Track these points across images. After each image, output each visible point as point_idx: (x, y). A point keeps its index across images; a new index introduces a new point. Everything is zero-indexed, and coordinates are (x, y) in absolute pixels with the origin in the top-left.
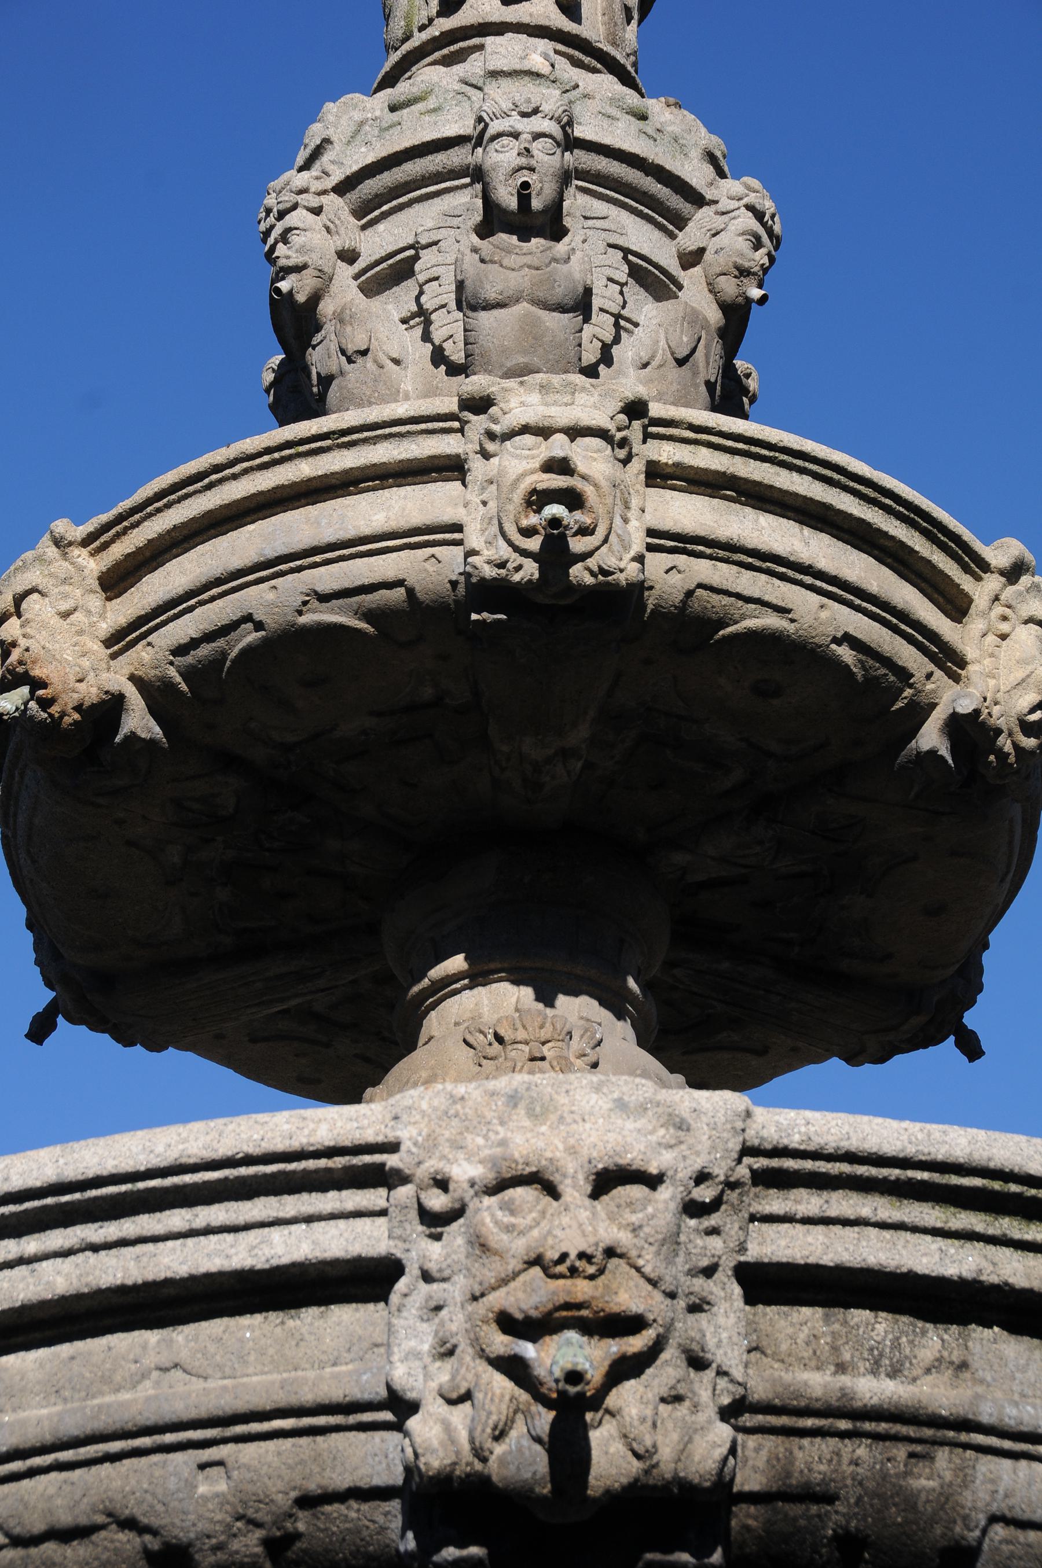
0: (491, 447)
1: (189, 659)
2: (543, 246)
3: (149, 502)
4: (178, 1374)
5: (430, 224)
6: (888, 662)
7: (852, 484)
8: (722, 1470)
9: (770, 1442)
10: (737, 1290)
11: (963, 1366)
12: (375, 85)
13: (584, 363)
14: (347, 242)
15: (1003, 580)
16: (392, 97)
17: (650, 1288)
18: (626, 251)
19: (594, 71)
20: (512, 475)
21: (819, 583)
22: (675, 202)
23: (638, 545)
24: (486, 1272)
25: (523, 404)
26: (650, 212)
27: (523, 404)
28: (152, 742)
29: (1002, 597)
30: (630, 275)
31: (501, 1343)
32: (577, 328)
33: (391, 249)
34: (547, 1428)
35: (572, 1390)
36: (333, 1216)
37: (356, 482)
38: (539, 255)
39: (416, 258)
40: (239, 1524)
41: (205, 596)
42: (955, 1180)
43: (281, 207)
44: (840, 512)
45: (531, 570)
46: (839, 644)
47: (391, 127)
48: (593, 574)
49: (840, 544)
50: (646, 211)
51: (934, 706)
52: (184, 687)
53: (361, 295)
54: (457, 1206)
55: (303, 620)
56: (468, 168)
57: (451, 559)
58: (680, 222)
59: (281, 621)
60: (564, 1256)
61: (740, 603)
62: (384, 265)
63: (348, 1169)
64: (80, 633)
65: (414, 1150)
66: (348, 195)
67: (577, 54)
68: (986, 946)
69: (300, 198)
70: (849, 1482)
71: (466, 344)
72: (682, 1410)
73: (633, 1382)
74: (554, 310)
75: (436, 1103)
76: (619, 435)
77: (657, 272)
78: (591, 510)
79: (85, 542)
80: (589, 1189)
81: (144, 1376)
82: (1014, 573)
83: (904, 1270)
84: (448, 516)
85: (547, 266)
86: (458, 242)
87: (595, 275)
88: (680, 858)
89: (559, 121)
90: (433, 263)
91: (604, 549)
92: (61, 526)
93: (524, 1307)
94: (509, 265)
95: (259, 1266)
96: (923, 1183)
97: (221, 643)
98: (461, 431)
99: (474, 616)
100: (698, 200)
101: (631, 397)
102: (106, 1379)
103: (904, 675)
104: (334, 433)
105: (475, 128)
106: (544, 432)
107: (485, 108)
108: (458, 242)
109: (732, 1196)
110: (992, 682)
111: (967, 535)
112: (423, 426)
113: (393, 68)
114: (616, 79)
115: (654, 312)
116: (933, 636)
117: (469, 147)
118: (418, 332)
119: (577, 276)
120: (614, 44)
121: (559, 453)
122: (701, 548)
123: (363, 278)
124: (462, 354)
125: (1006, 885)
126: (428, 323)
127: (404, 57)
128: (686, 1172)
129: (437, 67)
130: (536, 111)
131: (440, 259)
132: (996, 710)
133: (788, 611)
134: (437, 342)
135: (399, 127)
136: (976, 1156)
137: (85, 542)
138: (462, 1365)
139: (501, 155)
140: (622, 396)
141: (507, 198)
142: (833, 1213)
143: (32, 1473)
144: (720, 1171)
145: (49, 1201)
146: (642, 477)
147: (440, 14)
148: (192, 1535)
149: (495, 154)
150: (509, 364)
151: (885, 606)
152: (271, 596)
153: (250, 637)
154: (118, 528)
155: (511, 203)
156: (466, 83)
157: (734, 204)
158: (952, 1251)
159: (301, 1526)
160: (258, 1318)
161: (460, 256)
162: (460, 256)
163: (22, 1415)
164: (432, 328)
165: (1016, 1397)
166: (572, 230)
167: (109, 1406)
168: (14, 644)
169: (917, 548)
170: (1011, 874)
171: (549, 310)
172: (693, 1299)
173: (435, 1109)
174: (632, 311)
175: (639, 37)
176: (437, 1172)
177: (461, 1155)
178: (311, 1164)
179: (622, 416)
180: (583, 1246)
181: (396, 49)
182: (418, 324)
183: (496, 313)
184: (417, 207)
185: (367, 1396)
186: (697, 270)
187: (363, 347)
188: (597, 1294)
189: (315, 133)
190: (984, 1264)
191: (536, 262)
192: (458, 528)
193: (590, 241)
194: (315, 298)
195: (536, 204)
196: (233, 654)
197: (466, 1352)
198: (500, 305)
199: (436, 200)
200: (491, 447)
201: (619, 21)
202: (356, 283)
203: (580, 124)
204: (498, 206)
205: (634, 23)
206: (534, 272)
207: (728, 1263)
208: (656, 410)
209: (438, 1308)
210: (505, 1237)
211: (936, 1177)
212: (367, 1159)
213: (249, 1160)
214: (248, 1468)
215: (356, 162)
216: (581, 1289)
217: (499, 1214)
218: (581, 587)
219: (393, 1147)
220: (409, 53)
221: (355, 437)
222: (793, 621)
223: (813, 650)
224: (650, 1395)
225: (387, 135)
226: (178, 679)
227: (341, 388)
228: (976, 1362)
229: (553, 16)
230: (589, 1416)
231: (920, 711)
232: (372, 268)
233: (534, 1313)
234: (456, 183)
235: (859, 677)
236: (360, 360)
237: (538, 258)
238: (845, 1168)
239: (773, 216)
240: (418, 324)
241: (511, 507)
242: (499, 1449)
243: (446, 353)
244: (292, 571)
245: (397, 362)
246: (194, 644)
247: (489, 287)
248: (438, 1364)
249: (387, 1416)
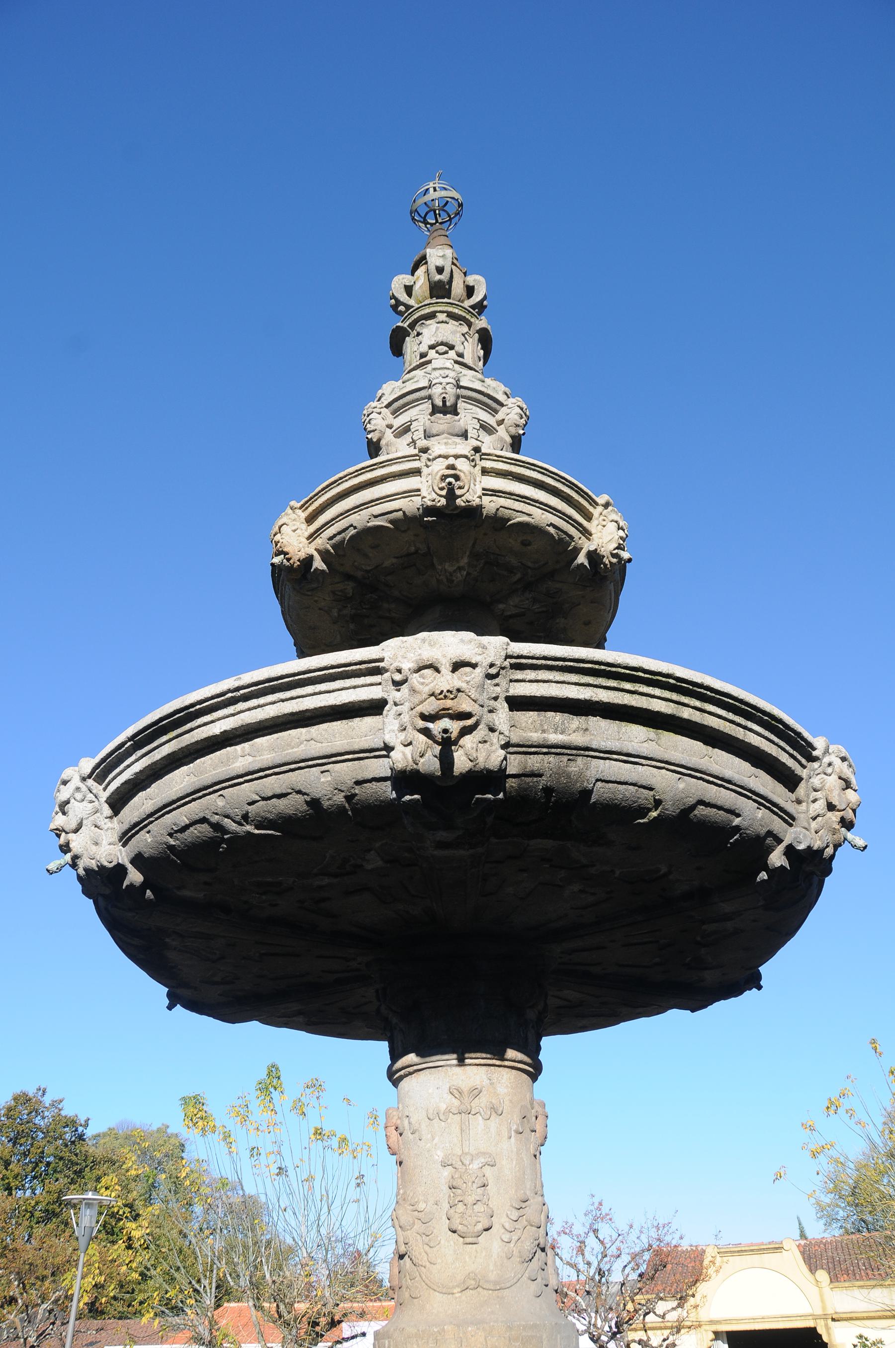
0: (429, 463)
1: (333, 541)
3: (320, 492)
4: (312, 742)
6: (566, 533)
7: (551, 475)
8: (501, 765)
9: (519, 757)
10: (506, 705)
11: (586, 730)
15: (603, 508)
17: (474, 703)
18: (479, 420)
20: (436, 471)
21: (541, 506)
22: (494, 405)
23: (480, 492)
24: (415, 699)
25: (439, 449)
27: (439, 449)
28: (323, 571)
29: (603, 514)
30: (480, 427)
31: (421, 724)
34: (438, 752)
35: (445, 736)
36: (363, 686)
37: (385, 479)
39: (411, 424)
40: (336, 791)
41: (338, 520)
42: (582, 665)
43: (368, 413)
44: (547, 484)
45: (443, 501)
46: (549, 526)
48: (464, 502)
49: (548, 494)
51: (582, 548)
52: (332, 551)
54: (405, 678)
55: (369, 525)
57: (417, 502)
58: (496, 412)
59: (362, 525)
60: (442, 692)
61: (515, 512)
62: (401, 428)
63: (367, 669)
64: (299, 536)
65: (389, 660)
68: (605, 640)
69: (374, 410)
70: (547, 769)
72: (487, 745)
73: (469, 736)
75: (396, 644)
76: (471, 458)
78: (463, 481)
79: (300, 508)
80: (451, 669)
81: (301, 743)
82: (606, 505)
83: (565, 697)
84: (415, 487)
88: (501, 606)
89: (455, 379)
91: (468, 493)
92: (293, 503)
93: (429, 710)
95: (338, 704)
96: (571, 666)
97: (343, 535)
98: (419, 460)
99: (425, 519)
100: (502, 405)
101: (475, 446)
102: (289, 745)
103: (571, 537)
106: (446, 457)
109: (502, 672)
110: (601, 540)
111: (590, 493)
112: (407, 459)
116: (580, 525)
119: (462, 425)
121: (451, 463)
122: (501, 494)
125: (610, 615)
126: (415, 444)
128: (486, 663)
130: (447, 376)
132: (602, 549)
133: (531, 515)
136: (589, 656)
137: (300, 508)
138: (408, 733)
141: (439, 403)
142: (539, 678)
143: (266, 776)
144: (498, 663)
145: (267, 685)
146: (480, 471)
148: (320, 795)
151: (564, 514)
152: (358, 517)
153: (352, 532)
154: (311, 502)
155: (441, 404)
157: (513, 405)
158: (582, 690)
159: (357, 791)
160: (339, 722)
163: (262, 757)
165: (605, 739)
167: (290, 753)
168: (278, 542)
169: (574, 496)
170: (612, 610)
172: (490, 708)
173: (396, 646)
176: (397, 667)
177: (405, 660)
178: (354, 667)
179: (472, 451)
180: (448, 688)
184: (411, 410)
185: (376, 746)
186: (502, 426)
188: (454, 705)
189: (380, 392)
190: (593, 694)
192: (419, 490)
194: (379, 440)
195: (448, 404)
196: (347, 539)
197: (410, 729)
198: (437, 435)
200: (429, 463)
207: (502, 696)
208: (484, 450)
209: (400, 715)
210: (421, 687)
211: (576, 664)
212: (374, 665)
213: (333, 667)
214: (337, 772)
216: (448, 703)
217: (419, 679)
218: (460, 507)
219: (381, 660)
221: (385, 464)
222: (533, 518)
223: (540, 528)
224: (475, 740)
226: (330, 548)
228: (591, 729)
230: (453, 748)
231: (577, 551)
233: (432, 713)
235: (557, 538)
238: (543, 662)
239: (526, 409)
241: (435, 481)
242: (422, 760)
244: (365, 508)
246: (335, 536)
248: (401, 733)
249: (384, 753)
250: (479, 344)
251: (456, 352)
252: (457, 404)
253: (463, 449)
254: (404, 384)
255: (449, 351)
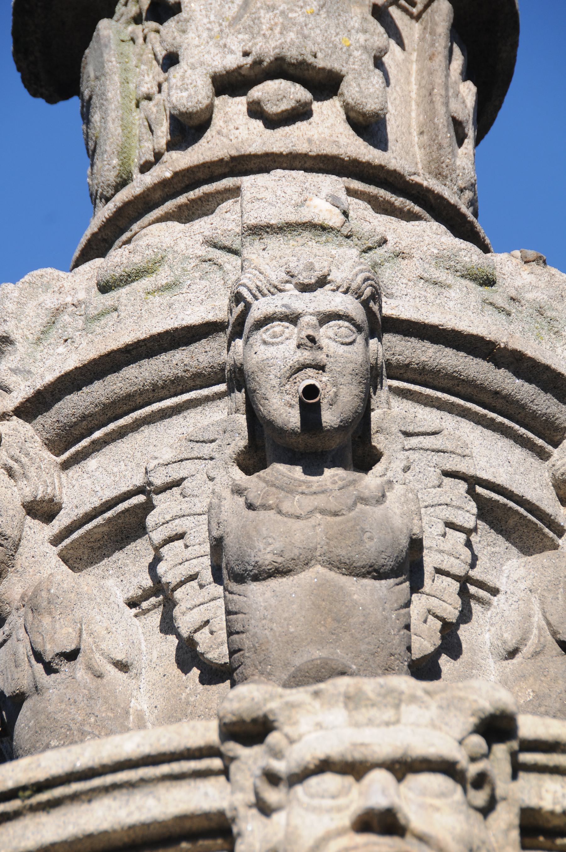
2: (342, 479)
5: (168, 455)
12: (77, 253)
13: (416, 654)
14: (41, 489)
16: (102, 272)
19: (410, 217)
25: (319, 726)
26: (506, 421)
27: (319, 726)
30: (481, 516)
32: (402, 601)
33: (108, 494)
38: (337, 493)
39: (148, 507)
47: (102, 314)
50: (500, 419)
53: (65, 567)
56: (223, 370)
62: (99, 520)
66: (40, 419)
67: (382, 193)
71: (230, 634)
74: (364, 576)
76: (473, 770)
77: (522, 510)
85: (350, 509)
86: (212, 479)
87: (426, 519)
90: (174, 512)
94: (291, 511)
98: (225, 772)
104: (24, 788)
105: (231, 311)
107: (245, 281)
108: (212, 479)
112: (165, 769)
113: (103, 227)
114: (443, 227)
115: (522, 572)
117: (223, 338)
118: (155, 618)
119: (398, 522)
120: (439, 175)
123: (67, 541)
124: (225, 650)
127: (120, 211)
129: (170, 223)
130: (322, 282)
131: (184, 506)
134: (185, 632)
135: (115, 314)
139: (272, 349)
140: (475, 706)
146: (515, 834)
147: (171, 146)
149: (263, 347)
150: (298, 661)
156: (215, 246)
161: (215, 501)
162: (215, 501)
164: (177, 612)
166: (386, 453)
171: (357, 575)
174: (486, 571)
175: (477, 161)
181: (108, 200)
182: (155, 607)
183: (274, 583)
184: (146, 431)
187: (69, 648)
191: (333, 505)
193: (415, 468)
199: (177, 420)
201: (445, 142)
202: (56, 550)
203: (390, 296)
204: (270, 423)
205: (469, 143)
206: (330, 519)
215: (51, 369)
220: (127, 205)
225: (97, 327)
227: (36, 713)
229: (343, 140)
232: (95, 517)
234: (205, 392)
236: (65, 667)
237: (336, 498)
240: (155, 607)
243: (200, 649)
245: (123, 666)
247: (261, 546)
250: (457, 50)
251: (348, 109)
252: (367, 410)
253: (433, 725)
254: (109, 299)
255: (316, 106)
